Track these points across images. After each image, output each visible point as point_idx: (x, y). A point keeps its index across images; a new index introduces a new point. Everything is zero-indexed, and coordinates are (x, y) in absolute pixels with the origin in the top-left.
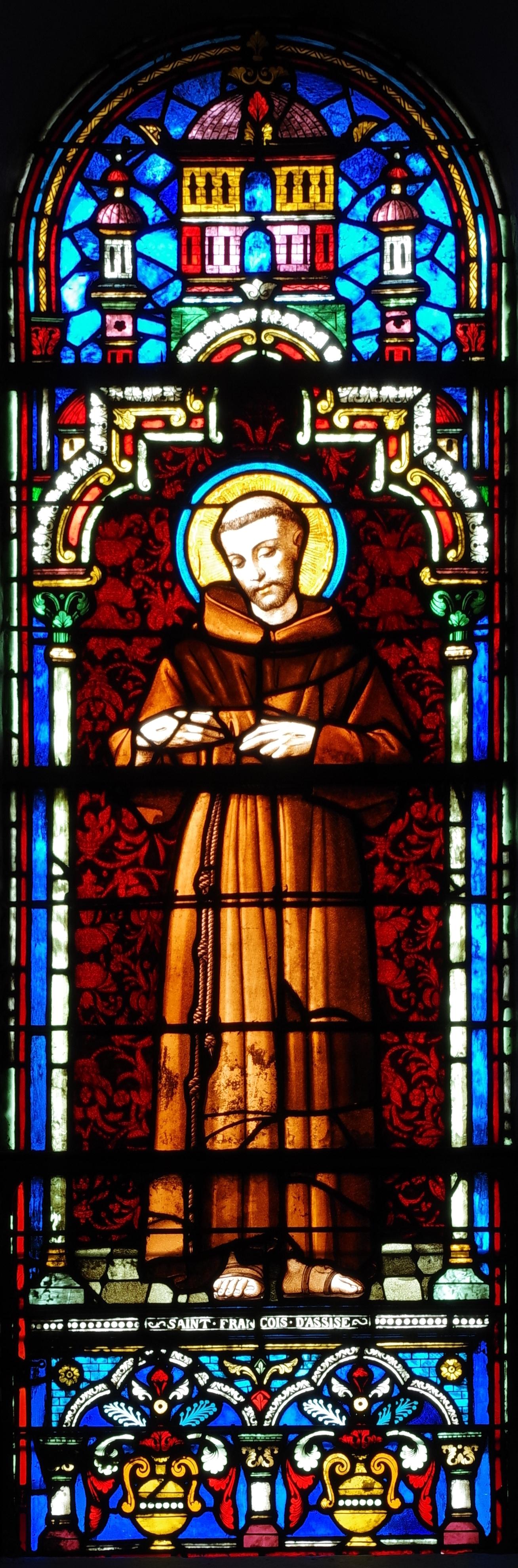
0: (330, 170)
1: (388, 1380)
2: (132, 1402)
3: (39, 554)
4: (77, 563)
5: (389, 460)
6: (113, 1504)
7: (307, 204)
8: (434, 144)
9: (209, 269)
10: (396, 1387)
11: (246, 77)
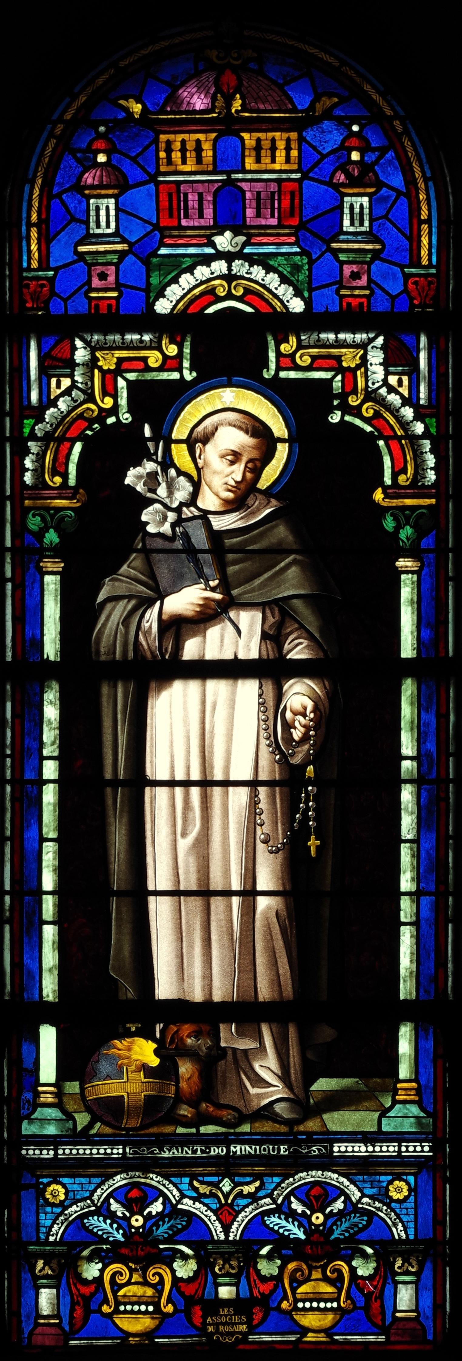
1: (161, 1200)
2: (291, 1215)
6: (94, 1307)
7: (200, 166)
10: (168, 1205)
11: (218, 57)
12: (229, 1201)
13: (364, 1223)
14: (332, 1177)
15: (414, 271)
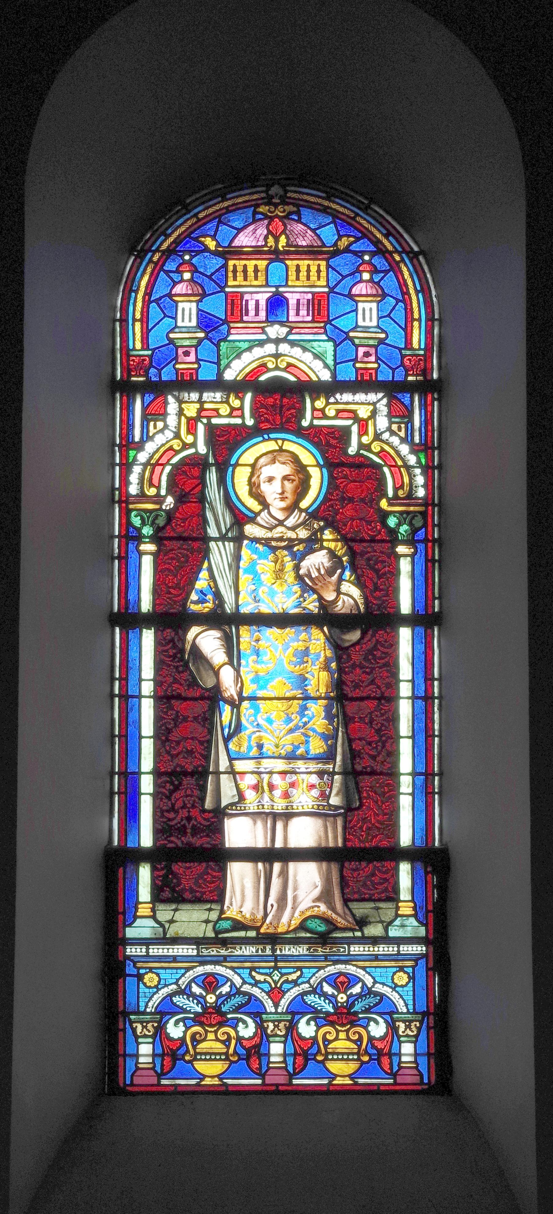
0: (323, 264)
3: (133, 490)
4: (158, 495)
5: (360, 435)
8: (391, 253)
9: (245, 318)
12: (278, 986)
13: (377, 1001)
14: (350, 969)
15: (408, 352)
